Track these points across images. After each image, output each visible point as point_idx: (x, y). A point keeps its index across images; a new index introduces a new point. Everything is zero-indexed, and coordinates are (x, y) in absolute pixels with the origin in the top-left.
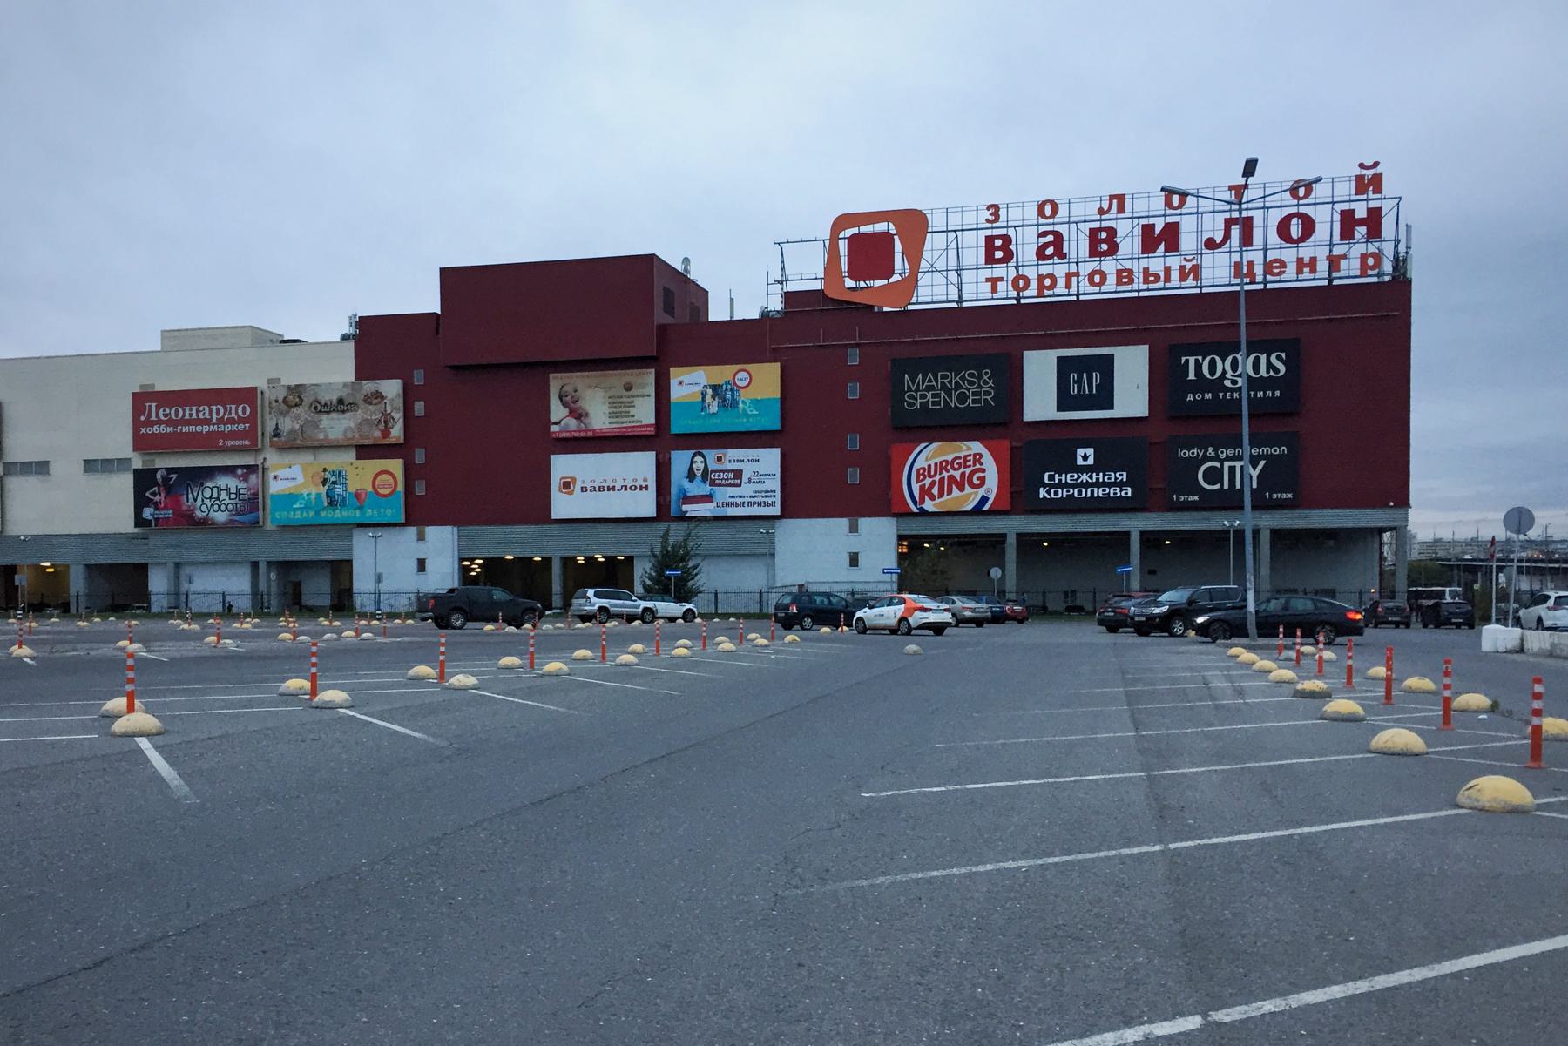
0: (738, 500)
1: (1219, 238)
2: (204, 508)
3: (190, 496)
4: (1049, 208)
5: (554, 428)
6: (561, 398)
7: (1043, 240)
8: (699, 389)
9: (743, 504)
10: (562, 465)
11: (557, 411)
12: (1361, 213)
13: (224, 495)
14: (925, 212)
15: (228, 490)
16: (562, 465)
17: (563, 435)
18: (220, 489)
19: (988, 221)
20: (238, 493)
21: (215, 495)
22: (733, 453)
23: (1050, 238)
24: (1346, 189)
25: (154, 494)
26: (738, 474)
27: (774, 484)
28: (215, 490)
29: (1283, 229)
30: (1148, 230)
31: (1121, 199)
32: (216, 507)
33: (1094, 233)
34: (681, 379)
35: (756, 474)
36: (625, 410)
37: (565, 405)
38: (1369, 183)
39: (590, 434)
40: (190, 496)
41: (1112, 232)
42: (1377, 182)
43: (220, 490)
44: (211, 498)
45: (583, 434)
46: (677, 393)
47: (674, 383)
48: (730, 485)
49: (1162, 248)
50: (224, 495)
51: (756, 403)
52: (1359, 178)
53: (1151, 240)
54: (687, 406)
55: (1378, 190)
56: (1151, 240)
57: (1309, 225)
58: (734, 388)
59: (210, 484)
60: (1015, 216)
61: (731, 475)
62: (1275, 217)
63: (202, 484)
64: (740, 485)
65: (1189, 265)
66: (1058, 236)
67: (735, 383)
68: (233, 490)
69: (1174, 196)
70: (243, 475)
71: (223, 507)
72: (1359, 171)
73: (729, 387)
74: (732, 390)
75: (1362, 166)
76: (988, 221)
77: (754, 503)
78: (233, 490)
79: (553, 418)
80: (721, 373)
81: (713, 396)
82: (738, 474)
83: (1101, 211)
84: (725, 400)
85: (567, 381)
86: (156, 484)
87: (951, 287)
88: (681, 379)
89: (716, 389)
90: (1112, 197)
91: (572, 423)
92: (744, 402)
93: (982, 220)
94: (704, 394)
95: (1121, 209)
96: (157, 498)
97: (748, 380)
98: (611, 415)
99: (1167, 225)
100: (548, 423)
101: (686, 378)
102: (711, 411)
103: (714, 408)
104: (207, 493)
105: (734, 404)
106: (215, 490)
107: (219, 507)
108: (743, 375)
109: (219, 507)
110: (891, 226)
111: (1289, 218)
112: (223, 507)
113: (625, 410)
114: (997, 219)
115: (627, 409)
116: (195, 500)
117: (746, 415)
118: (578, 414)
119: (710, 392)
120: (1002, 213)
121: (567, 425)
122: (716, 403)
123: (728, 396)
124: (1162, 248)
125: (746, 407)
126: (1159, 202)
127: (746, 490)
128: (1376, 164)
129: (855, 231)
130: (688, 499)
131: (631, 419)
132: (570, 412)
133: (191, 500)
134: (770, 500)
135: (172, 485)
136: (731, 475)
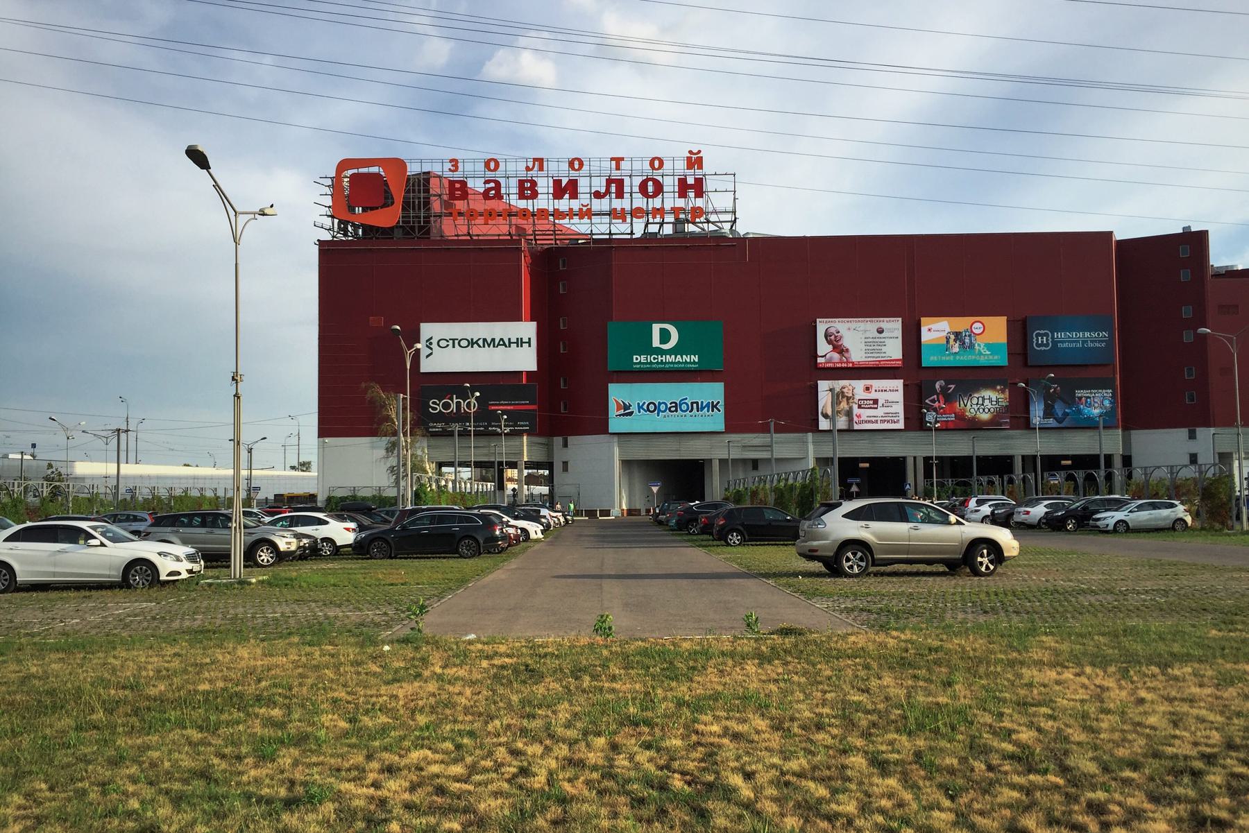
0: (873, 419)
1: (603, 190)
2: (972, 410)
3: (962, 402)
4: (491, 164)
5: (820, 360)
6: (826, 336)
7: (488, 186)
8: (945, 334)
9: (877, 422)
10: (617, 393)
11: (823, 348)
12: (691, 181)
13: (987, 402)
14: (640, 195)
15: (990, 399)
16: (617, 393)
17: (828, 365)
18: (984, 399)
19: (450, 170)
20: (997, 401)
21: (980, 402)
22: (876, 384)
23: (492, 185)
24: (681, 166)
25: (933, 401)
26: (876, 401)
27: (899, 409)
28: (980, 399)
29: (643, 188)
30: (557, 183)
31: (541, 161)
32: (981, 411)
33: (521, 183)
34: (930, 327)
35: (887, 401)
36: (878, 348)
37: (829, 342)
38: (695, 161)
39: (850, 365)
40: (962, 402)
41: (534, 184)
42: (700, 165)
43: (984, 399)
44: (977, 404)
45: (843, 365)
46: (926, 336)
47: (924, 330)
48: (871, 408)
49: (567, 196)
50: (987, 402)
51: (988, 346)
52: (689, 159)
53: (559, 191)
54: (934, 347)
55: (700, 167)
56: (559, 191)
57: (659, 188)
58: (971, 334)
59: (977, 395)
60: (469, 167)
61: (872, 402)
62: (637, 181)
63: (971, 395)
64: (877, 408)
65: (585, 209)
66: (498, 184)
67: (972, 331)
68: (994, 399)
69: (575, 163)
70: (1001, 390)
71: (986, 410)
72: (689, 155)
73: (967, 334)
74: (970, 336)
75: (690, 152)
76: (450, 170)
77: (885, 421)
78: (994, 399)
79: (819, 353)
80: (962, 323)
81: (955, 341)
82: (876, 401)
83: (528, 169)
84: (964, 343)
85: (832, 324)
86: (935, 392)
87: (191, 481)
88: (930, 327)
89: (958, 335)
90: (535, 160)
91: (836, 356)
92: (979, 345)
93: (446, 169)
94: (948, 339)
95: (541, 169)
96: (936, 404)
97: (982, 330)
98: (867, 351)
99: (570, 181)
100: (816, 356)
101: (933, 327)
102: (954, 351)
103: (956, 348)
104: (975, 401)
105: (972, 346)
106: (980, 399)
107: (984, 410)
108: (977, 325)
109: (984, 410)
110: (381, 170)
111: (578, 170)
112: (986, 410)
113: (878, 348)
114: (456, 170)
115: (880, 347)
116: (966, 406)
117: (980, 354)
118: (839, 349)
119: (953, 337)
120: (460, 165)
121: (831, 358)
122: (957, 345)
123: (967, 340)
124: (567, 196)
125: (981, 349)
126: (566, 166)
127: (880, 412)
128: (699, 152)
129: (355, 171)
130: (861, 422)
131: (884, 355)
132: (834, 348)
133: (962, 405)
134: (895, 419)
135: (949, 394)
136: (872, 402)
